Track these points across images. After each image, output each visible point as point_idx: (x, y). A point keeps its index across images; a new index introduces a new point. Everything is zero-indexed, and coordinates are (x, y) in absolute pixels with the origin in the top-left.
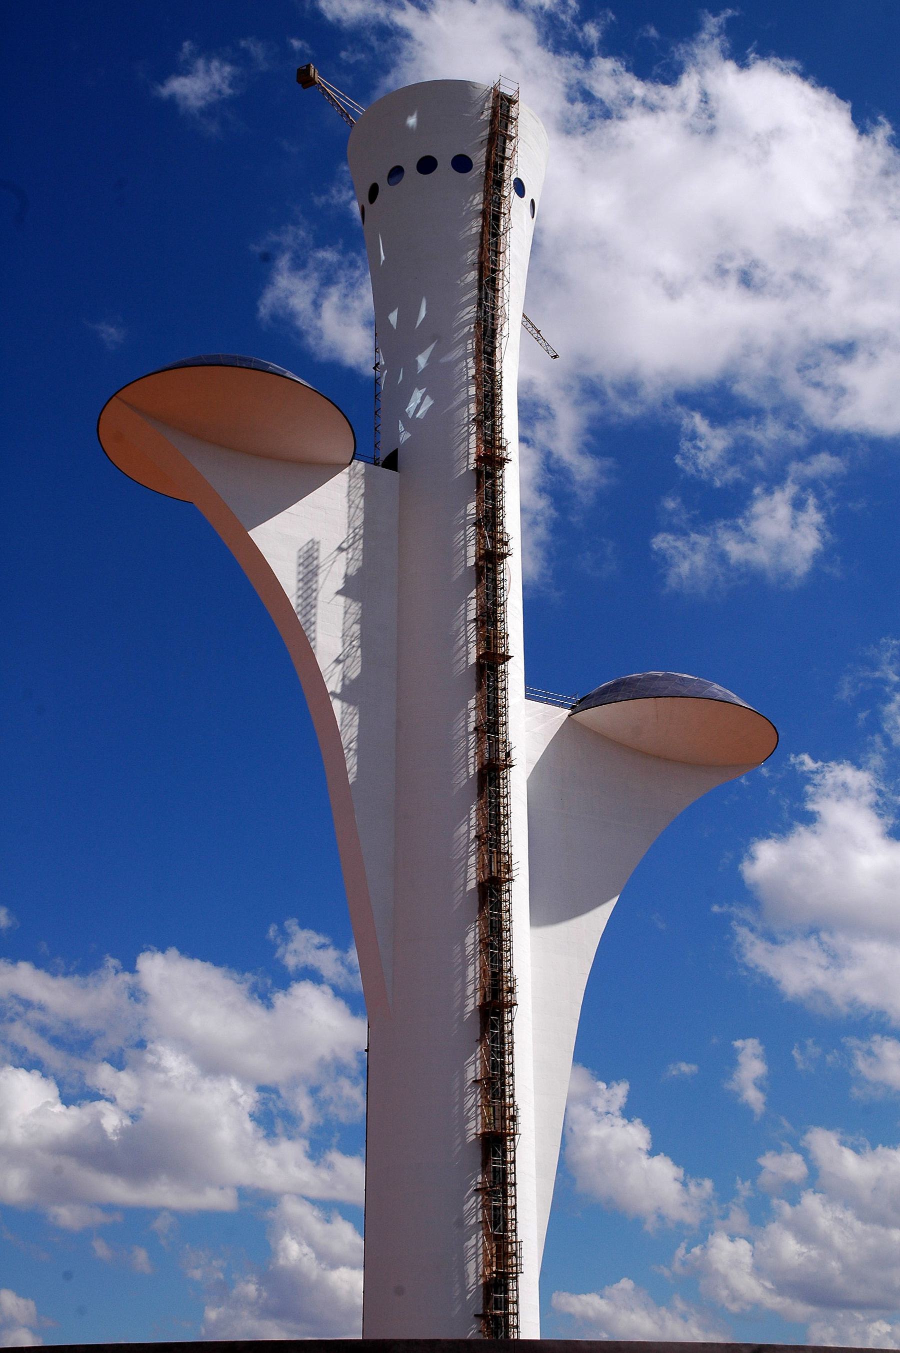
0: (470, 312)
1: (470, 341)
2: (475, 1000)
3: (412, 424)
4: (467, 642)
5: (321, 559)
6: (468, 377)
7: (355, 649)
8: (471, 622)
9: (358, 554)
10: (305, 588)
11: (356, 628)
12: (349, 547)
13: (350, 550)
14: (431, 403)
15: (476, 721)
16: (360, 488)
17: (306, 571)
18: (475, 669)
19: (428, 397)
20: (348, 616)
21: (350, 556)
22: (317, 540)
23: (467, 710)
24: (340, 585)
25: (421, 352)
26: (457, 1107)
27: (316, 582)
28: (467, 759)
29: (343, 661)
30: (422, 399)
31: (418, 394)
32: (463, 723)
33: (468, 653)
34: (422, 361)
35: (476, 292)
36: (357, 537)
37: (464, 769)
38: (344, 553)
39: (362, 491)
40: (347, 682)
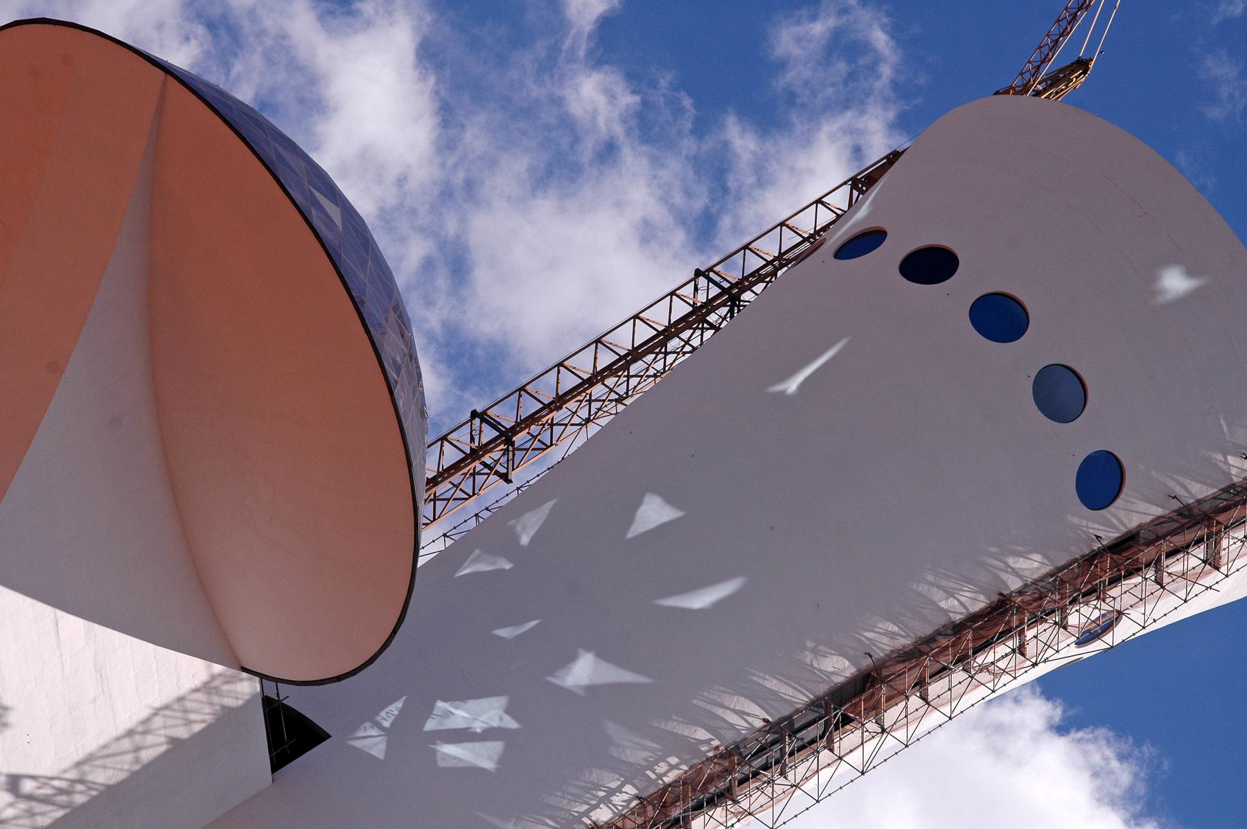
0: (747, 717)
1: (674, 760)
3: (411, 738)
6: (586, 814)
13: (23, 805)
14: (489, 765)
16: (189, 723)
19: (496, 747)
25: (605, 654)
30: (490, 734)
31: (488, 712)
34: (583, 671)
35: (801, 698)
36: (62, 799)
39: (182, 733)
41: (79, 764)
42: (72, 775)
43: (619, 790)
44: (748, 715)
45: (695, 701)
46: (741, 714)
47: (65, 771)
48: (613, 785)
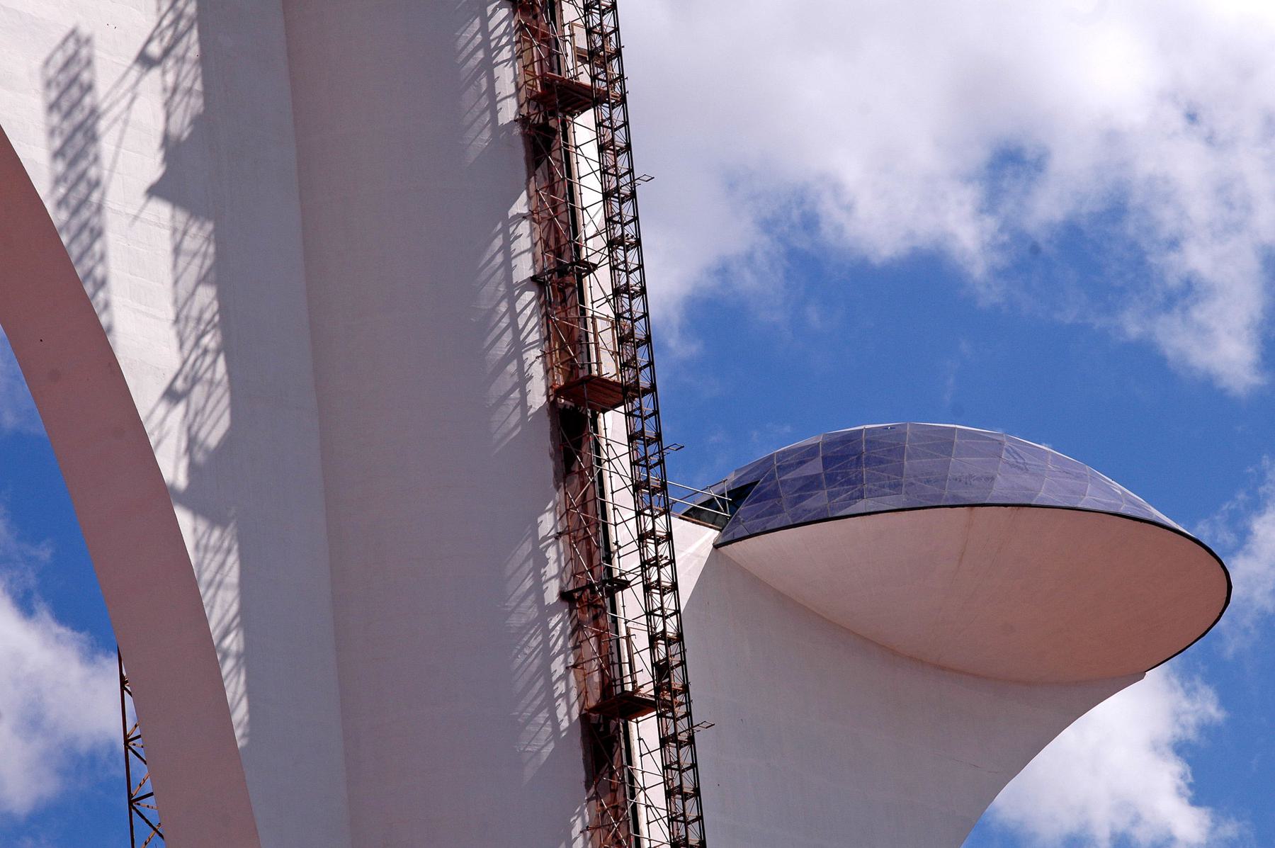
2: (570, 707)
4: (519, 347)
5: (103, 86)
7: (208, 359)
8: (524, 287)
9: (191, 77)
10: (72, 176)
11: (206, 295)
13: (170, 63)
15: (559, 576)
17: (67, 126)
18: (546, 425)
19: (490, 29)
20: (182, 261)
21: (170, 78)
22: (85, 31)
23: (536, 542)
24: (152, 167)
27: (96, 159)
28: (549, 685)
29: (185, 394)
32: (528, 583)
33: (523, 379)
36: (183, 24)
37: (544, 714)
38: (155, 73)
40: (200, 457)
47: (159, 9)
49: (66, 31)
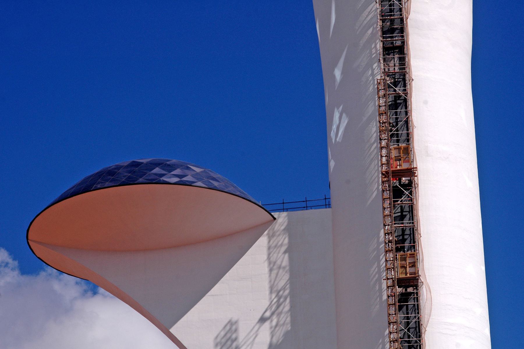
12: (273, 314)
19: (344, 115)
21: (274, 323)
22: (234, 320)
26: (381, 346)
41: (271, 292)
42: (274, 296)
43: (373, 70)
44: (371, 10)
45: (358, 33)
46: (369, 13)
47: (271, 298)
48: (370, 72)
49: (227, 321)
